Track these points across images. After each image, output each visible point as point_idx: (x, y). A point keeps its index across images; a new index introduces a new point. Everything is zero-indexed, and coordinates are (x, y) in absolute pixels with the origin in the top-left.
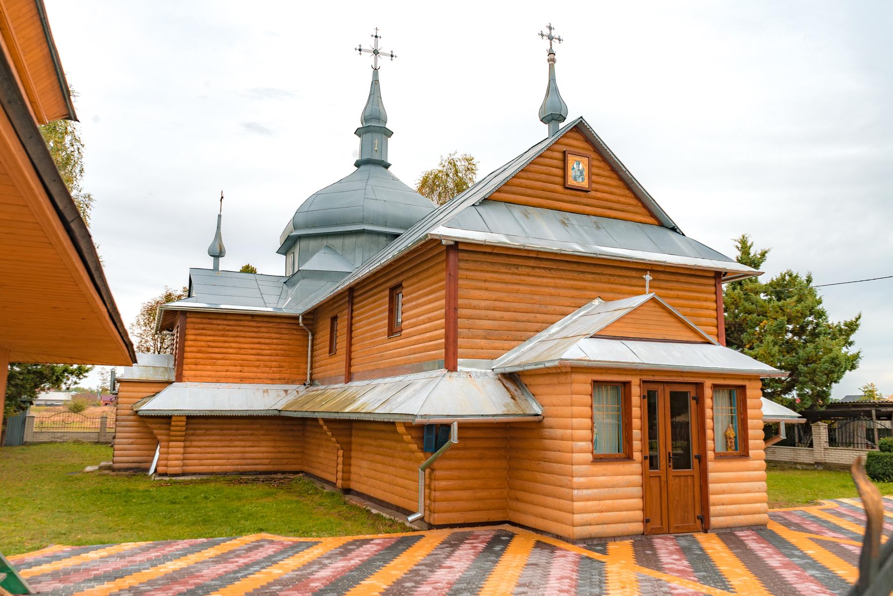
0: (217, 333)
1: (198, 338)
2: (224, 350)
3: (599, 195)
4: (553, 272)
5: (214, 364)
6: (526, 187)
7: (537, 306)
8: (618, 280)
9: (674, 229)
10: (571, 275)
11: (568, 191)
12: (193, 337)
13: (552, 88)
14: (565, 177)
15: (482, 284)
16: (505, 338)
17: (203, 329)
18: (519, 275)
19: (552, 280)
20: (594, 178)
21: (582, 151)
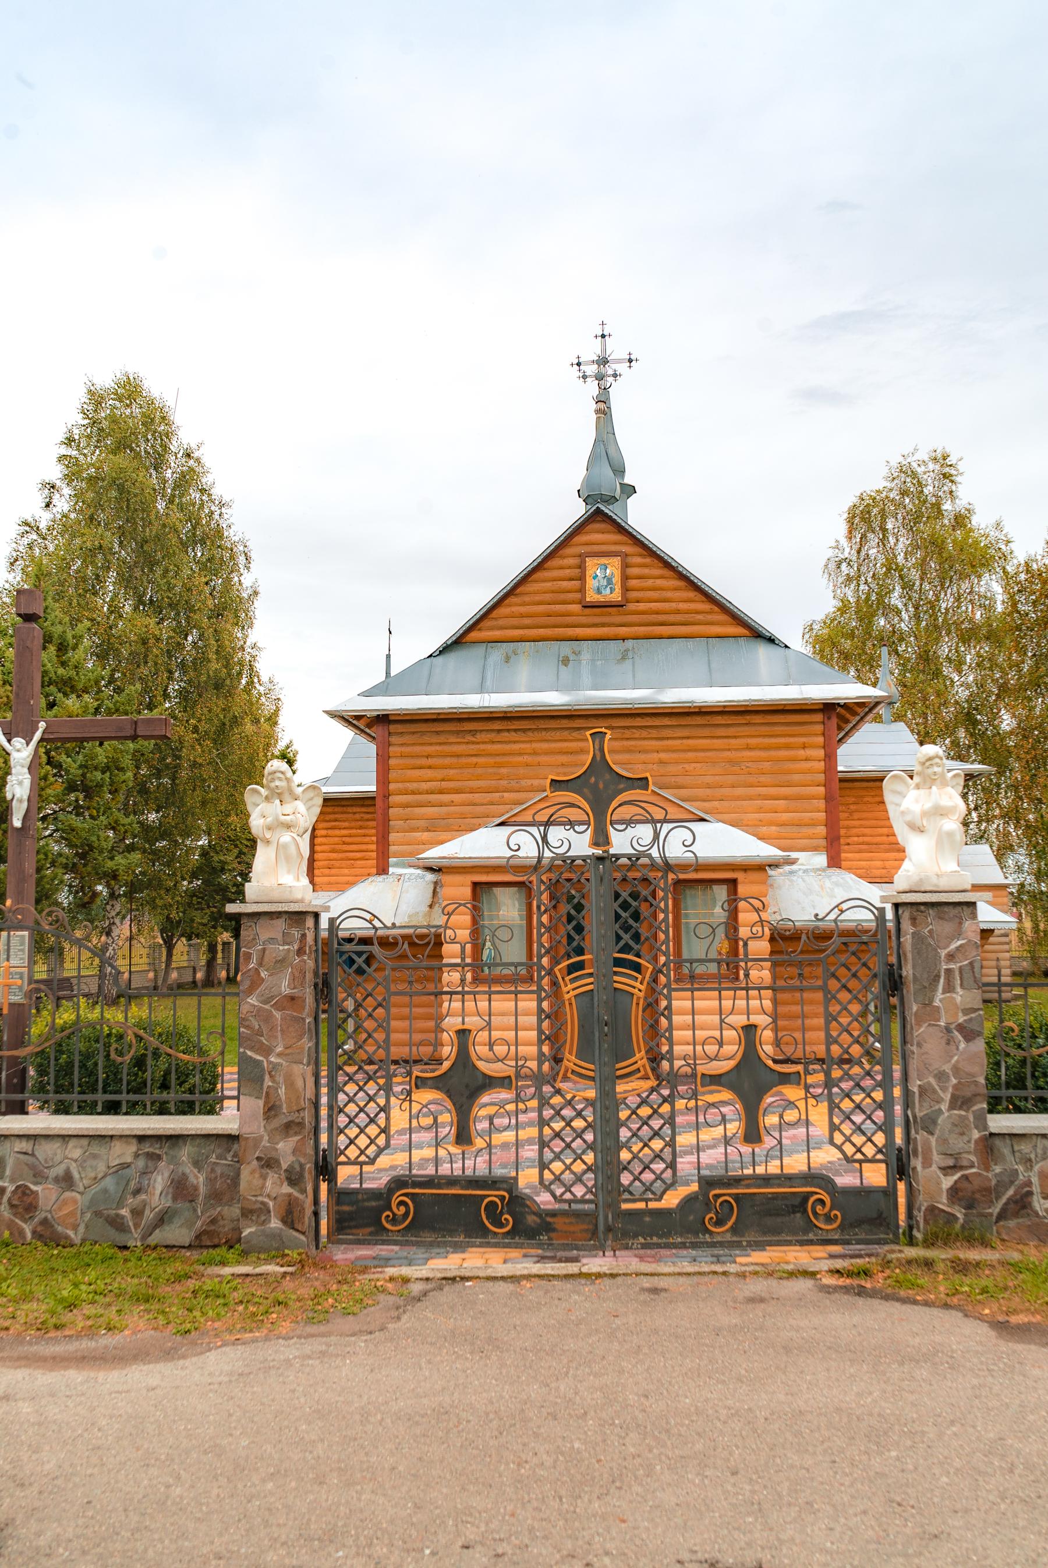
0: (353, 824)
1: (330, 832)
2: (364, 847)
3: (642, 606)
4: (530, 734)
5: (353, 867)
6: (522, 616)
7: (504, 783)
8: (637, 733)
9: (771, 640)
10: (558, 735)
11: (588, 611)
12: (324, 832)
13: (606, 453)
14: (582, 590)
15: (423, 761)
16: (456, 828)
17: (336, 820)
18: (478, 743)
19: (528, 746)
20: (633, 583)
21: (613, 548)
